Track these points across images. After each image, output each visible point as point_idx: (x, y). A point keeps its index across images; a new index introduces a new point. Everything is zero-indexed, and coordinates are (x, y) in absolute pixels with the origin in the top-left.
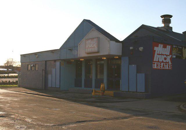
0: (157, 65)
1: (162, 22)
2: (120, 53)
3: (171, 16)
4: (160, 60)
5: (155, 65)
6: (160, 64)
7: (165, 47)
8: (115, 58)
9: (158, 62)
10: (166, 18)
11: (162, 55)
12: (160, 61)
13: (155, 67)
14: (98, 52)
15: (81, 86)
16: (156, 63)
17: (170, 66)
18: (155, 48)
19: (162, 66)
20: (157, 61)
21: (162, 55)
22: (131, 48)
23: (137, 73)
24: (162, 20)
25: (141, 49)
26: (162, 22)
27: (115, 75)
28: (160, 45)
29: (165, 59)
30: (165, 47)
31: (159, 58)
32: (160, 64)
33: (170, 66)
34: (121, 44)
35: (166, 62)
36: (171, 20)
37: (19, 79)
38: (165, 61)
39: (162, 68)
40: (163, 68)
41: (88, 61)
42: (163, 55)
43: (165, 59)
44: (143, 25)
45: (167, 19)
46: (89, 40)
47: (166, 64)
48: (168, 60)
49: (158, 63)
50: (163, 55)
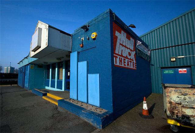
0: (121, 61)
5: (118, 60)
8: (180, 123)
9: (122, 56)
13: (118, 64)
15: (55, 88)
23: (88, 73)
31: (122, 50)
32: (124, 60)
33: (134, 66)
39: (126, 66)
40: (128, 67)
42: (128, 48)
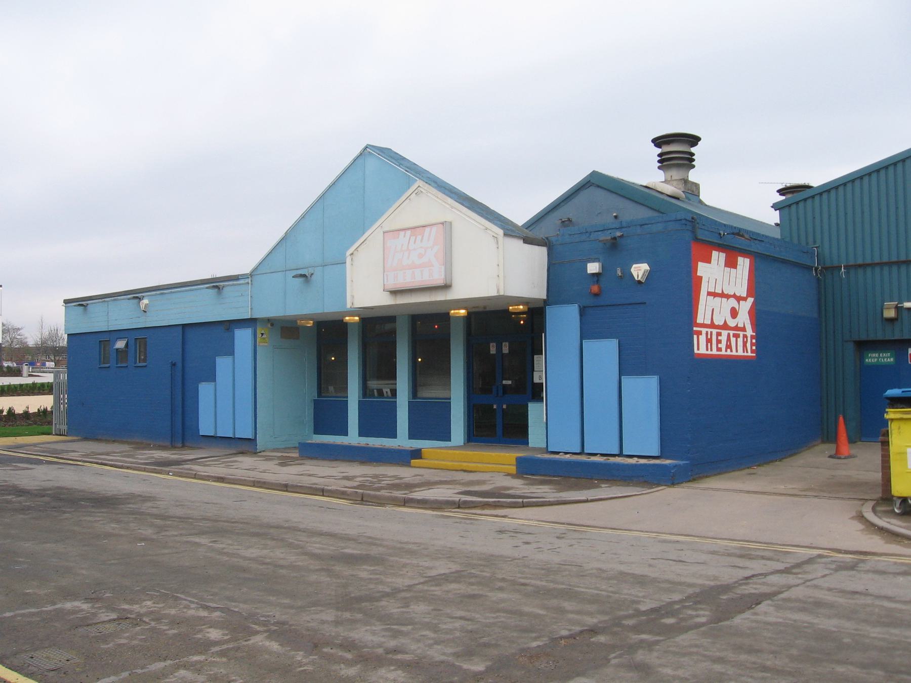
1: (659, 161)
2: (544, 296)
3: (694, 140)
4: (719, 321)
5: (703, 338)
6: (719, 334)
7: (731, 263)
9: (712, 325)
10: (666, 148)
11: (722, 295)
12: (716, 324)
13: (703, 350)
14: (446, 287)
16: (704, 330)
17: (749, 345)
18: (703, 269)
19: (723, 346)
20: (708, 322)
21: (722, 295)
22: (593, 268)
24: (659, 155)
25: (639, 270)
26: (659, 161)
27: (504, 382)
28: (715, 254)
29: (734, 313)
30: (731, 263)
32: (719, 334)
33: (749, 345)
34: (544, 250)
35: (736, 328)
36: (693, 154)
37: (57, 401)
38: (732, 323)
39: (723, 352)
40: (729, 353)
41: (377, 328)
42: (728, 297)
43: (734, 313)
44: (594, 174)
45: (677, 150)
46: (402, 233)
47: (736, 336)
48: (744, 319)
49: (709, 330)
50: (728, 297)
